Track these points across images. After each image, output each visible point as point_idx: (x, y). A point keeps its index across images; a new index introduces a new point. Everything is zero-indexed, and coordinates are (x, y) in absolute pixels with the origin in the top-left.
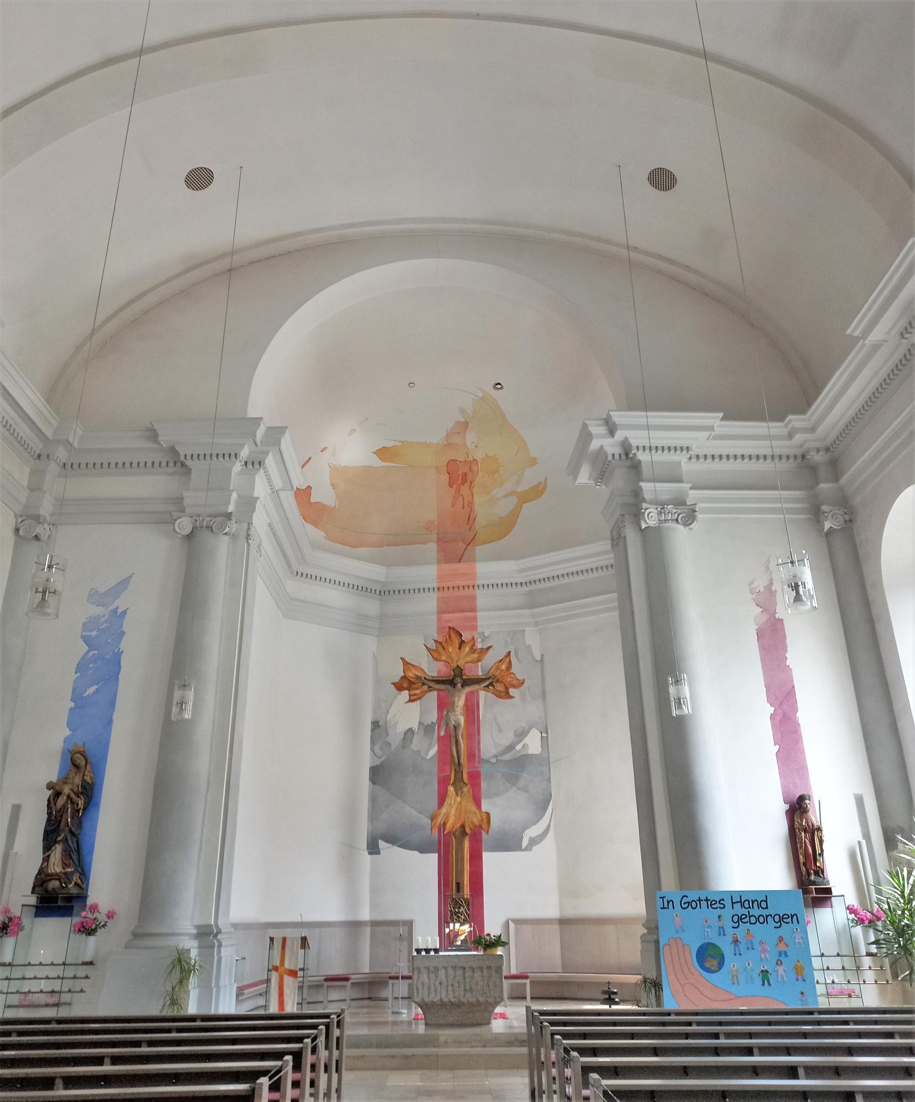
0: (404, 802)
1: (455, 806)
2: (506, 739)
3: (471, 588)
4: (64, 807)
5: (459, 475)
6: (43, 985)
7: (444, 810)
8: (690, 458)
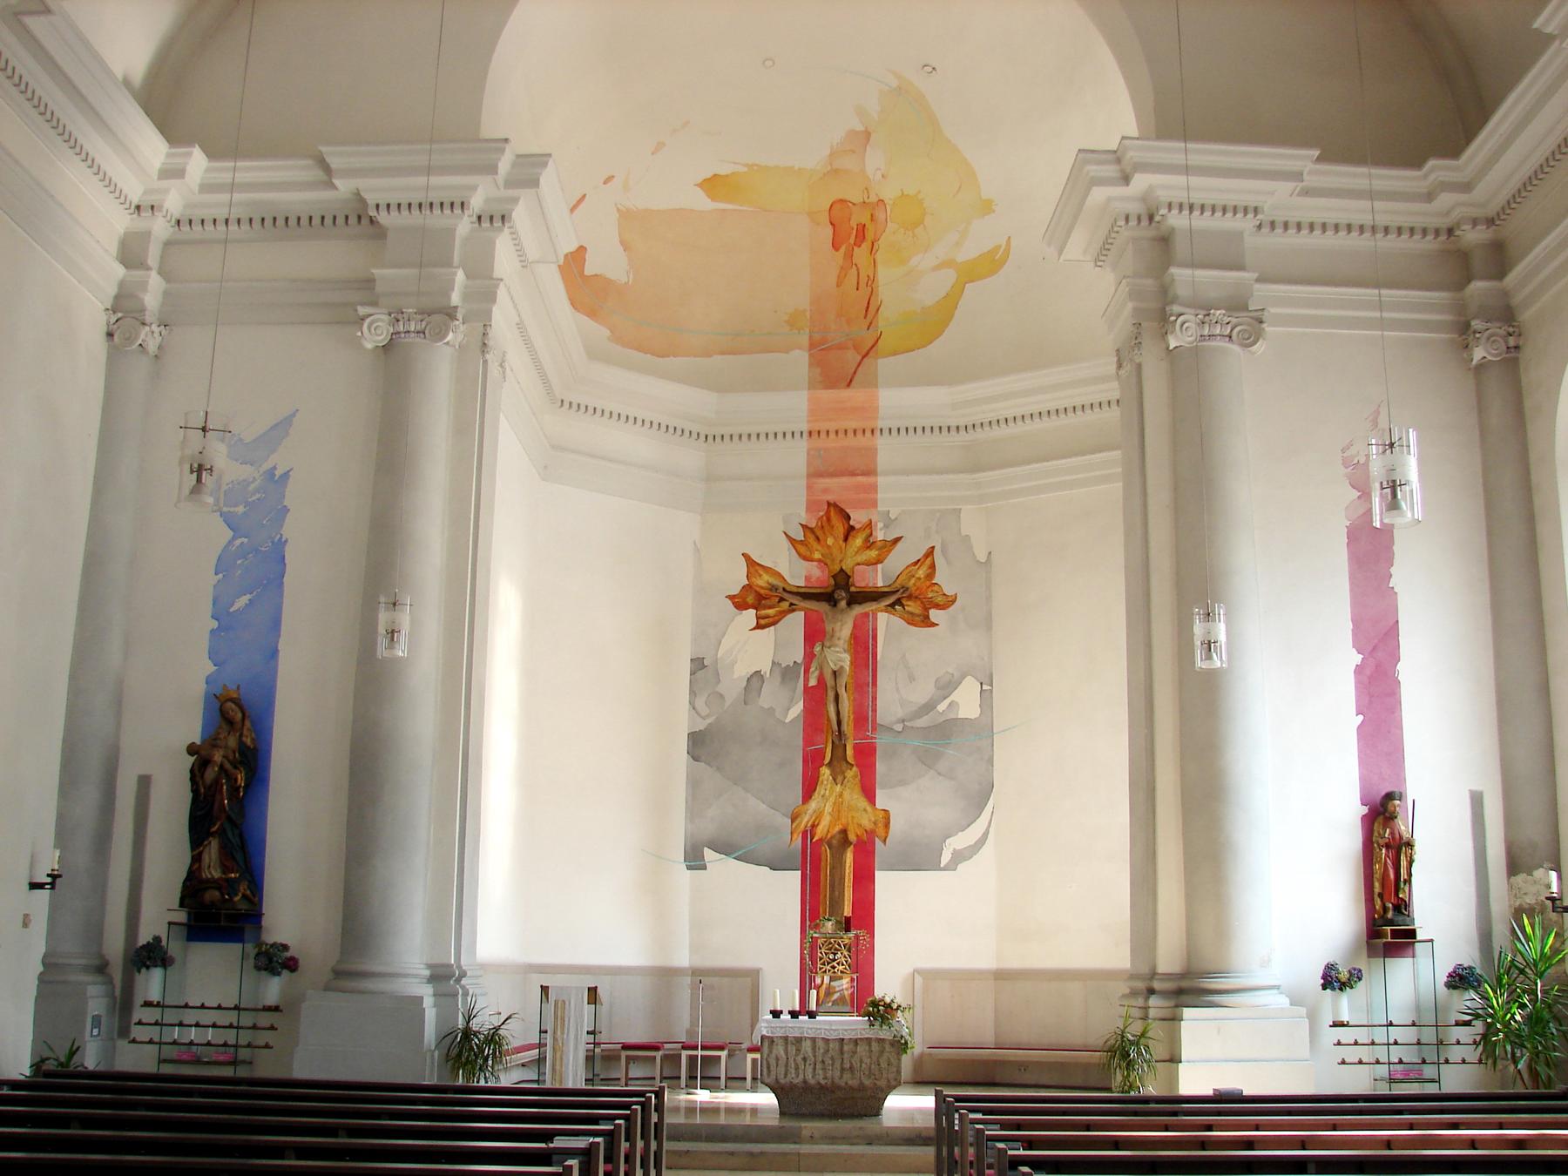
0: (746, 790)
1: (832, 799)
2: (920, 693)
3: (868, 434)
4: (217, 781)
5: (852, 231)
6: (210, 1034)
7: (813, 805)
8: (1260, 227)
